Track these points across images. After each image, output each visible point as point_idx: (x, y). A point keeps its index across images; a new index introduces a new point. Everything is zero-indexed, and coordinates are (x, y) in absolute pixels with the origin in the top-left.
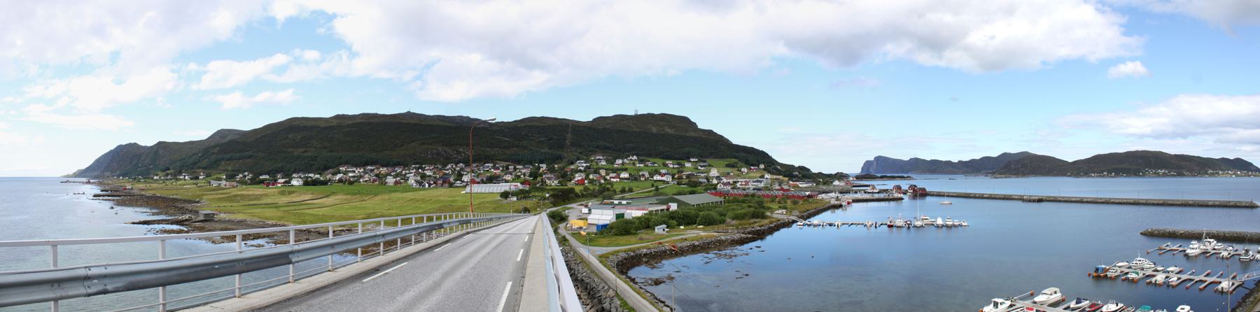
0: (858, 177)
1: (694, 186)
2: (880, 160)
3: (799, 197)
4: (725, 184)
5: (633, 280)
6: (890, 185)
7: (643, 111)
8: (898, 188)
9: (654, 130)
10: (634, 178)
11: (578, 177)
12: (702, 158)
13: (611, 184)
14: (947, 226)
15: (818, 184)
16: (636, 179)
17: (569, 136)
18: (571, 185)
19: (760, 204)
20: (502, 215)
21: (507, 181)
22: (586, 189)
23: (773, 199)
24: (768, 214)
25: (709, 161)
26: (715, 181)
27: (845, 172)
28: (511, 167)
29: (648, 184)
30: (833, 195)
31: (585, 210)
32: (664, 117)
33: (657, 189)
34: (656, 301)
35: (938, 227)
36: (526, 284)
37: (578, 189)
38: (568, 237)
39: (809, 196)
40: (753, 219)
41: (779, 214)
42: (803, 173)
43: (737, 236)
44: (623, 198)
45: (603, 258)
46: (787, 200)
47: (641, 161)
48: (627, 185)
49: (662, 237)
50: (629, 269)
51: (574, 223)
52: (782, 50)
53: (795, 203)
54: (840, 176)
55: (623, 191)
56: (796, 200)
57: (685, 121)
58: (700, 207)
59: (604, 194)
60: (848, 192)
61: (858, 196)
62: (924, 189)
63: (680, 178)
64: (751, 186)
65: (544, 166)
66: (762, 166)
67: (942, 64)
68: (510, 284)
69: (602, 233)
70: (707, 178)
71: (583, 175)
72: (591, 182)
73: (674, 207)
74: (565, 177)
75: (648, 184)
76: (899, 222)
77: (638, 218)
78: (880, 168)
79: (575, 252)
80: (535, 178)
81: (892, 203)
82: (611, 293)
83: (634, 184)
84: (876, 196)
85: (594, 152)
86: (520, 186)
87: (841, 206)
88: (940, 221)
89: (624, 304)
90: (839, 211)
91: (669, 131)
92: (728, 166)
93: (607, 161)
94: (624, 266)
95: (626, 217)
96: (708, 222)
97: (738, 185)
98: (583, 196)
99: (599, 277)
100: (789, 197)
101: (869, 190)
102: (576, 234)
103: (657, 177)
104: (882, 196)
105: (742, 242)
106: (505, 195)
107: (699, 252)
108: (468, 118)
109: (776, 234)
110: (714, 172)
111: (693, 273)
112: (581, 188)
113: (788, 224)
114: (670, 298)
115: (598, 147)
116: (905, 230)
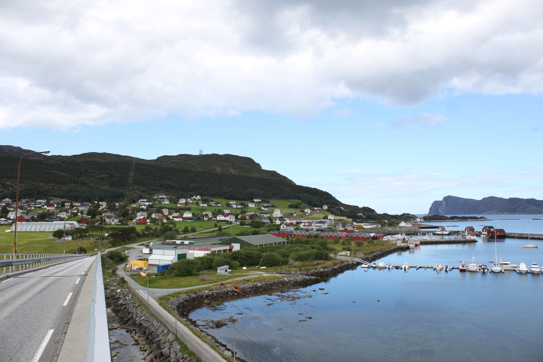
0: (426, 218)
1: (257, 226)
2: (448, 199)
3: (363, 239)
4: (288, 225)
5: (194, 323)
6: (461, 226)
7: (208, 151)
8: (471, 230)
9: (218, 170)
10: (197, 218)
11: (140, 216)
12: (265, 198)
13: (174, 223)
14: (533, 273)
15: (383, 225)
16: (199, 219)
17: (132, 173)
18: (132, 224)
19: (324, 245)
20: (52, 256)
21: (61, 219)
22: (148, 228)
23: (337, 240)
24: (332, 255)
25: (273, 202)
26: (278, 222)
27: (412, 212)
28: (67, 205)
29: (212, 224)
30: (399, 236)
31: (146, 251)
32: (228, 157)
33: (220, 229)
34: (217, 344)
35: (521, 273)
36: (70, 330)
37: (139, 228)
38: (127, 279)
39: (374, 238)
40: (317, 261)
41: (343, 256)
42: (368, 214)
43: (300, 278)
44: (185, 238)
45: (163, 301)
46: (350, 241)
47: (204, 201)
48: (190, 225)
49: (224, 278)
50: (190, 311)
51: (134, 263)
52: (342, 90)
53: (359, 245)
54: (406, 217)
55: (186, 231)
56: (360, 241)
57: (249, 162)
58: (263, 248)
59: (166, 234)
60: (415, 234)
61: (427, 238)
62: (502, 231)
63: (243, 218)
64: (315, 226)
65: (104, 204)
66: (325, 207)
67: (515, 91)
68: (51, 332)
69: (163, 274)
70: (270, 219)
71: (145, 214)
72: (153, 221)
73: (236, 247)
74: (126, 215)
75: (212, 224)
76: (473, 267)
77: (200, 259)
78: (450, 209)
79: (134, 295)
80: (94, 216)
81: (466, 246)
82: (171, 337)
83: (196, 224)
84: (447, 238)
85: (157, 191)
86: (76, 225)
87: (408, 248)
88: (523, 267)
89: (184, 348)
90: (406, 254)
91: (233, 171)
92: (291, 206)
93: (170, 200)
94: (184, 309)
95: (189, 257)
96: (271, 263)
97: (301, 226)
98: (144, 235)
99: (158, 320)
100: (353, 239)
101: (438, 231)
102: (136, 275)
103: (220, 218)
104: (452, 238)
105: (305, 284)
106: (59, 234)
107: (261, 293)
108: (19, 149)
109: (340, 276)
110: (277, 213)
111: (258, 316)
112: (143, 227)
113: (353, 266)
114: (229, 341)
115: (161, 186)
116: (479, 275)
